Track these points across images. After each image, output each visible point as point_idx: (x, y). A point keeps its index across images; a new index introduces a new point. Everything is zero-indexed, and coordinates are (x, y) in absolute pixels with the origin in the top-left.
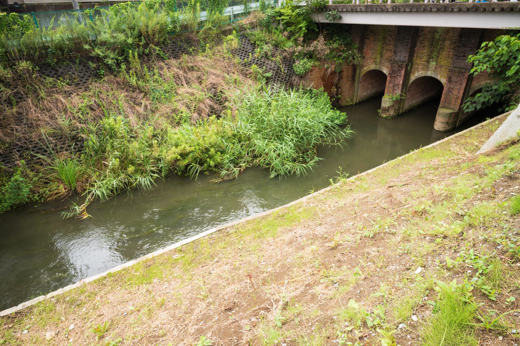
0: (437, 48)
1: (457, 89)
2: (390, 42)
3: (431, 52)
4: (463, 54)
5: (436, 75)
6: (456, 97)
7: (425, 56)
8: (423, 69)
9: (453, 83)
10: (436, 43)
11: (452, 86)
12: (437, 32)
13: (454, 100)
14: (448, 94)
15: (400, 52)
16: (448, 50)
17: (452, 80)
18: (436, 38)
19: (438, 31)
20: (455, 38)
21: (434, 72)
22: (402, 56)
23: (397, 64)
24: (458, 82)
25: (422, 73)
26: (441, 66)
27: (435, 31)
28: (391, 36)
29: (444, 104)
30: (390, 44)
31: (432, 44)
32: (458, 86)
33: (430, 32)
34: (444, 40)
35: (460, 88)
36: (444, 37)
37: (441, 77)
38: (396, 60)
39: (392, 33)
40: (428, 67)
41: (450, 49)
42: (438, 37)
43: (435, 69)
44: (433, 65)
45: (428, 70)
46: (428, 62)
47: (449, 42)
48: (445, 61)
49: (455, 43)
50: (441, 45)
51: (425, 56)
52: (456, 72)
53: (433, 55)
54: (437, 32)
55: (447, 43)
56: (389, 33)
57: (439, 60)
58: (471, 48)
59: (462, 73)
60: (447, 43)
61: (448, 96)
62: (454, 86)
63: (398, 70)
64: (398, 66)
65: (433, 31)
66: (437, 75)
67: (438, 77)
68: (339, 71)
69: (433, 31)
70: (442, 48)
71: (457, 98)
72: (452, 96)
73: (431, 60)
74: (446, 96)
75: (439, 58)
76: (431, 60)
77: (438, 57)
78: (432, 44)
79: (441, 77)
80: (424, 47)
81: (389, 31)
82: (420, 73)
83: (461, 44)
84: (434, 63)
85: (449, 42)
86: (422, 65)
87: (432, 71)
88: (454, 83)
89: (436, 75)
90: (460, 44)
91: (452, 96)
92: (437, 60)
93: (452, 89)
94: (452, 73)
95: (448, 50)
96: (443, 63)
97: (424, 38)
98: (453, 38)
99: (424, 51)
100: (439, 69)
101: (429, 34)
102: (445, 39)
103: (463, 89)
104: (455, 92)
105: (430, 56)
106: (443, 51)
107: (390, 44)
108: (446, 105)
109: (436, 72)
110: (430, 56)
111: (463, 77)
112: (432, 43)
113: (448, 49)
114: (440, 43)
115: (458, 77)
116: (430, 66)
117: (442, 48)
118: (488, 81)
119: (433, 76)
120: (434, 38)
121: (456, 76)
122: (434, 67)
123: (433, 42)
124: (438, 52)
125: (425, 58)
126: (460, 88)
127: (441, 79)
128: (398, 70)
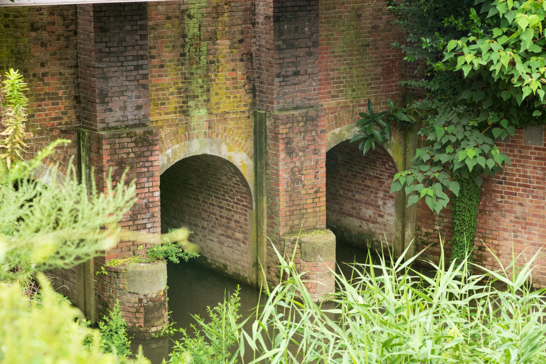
0: (198, 63)
1: (311, 168)
2: (43, 65)
3: (186, 80)
4: (294, 69)
5: (214, 147)
6: (312, 191)
7: (172, 94)
8: (176, 137)
9: (297, 155)
10: (192, 49)
11: (298, 164)
12: (190, 17)
13: (310, 201)
14: (293, 189)
15: (122, 93)
16: (230, 66)
17: (294, 145)
18: (190, 35)
19: (192, 12)
20: (240, 28)
21: (207, 140)
22: (129, 105)
23: (129, 135)
24: (307, 148)
25: (174, 152)
26: (224, 117)
27: (183, 12)
28: (43, 45)
29: (290, 223)
30: (44, 75)
31: (183, 55)
32: (310, 160)
33: (169, 18)
34: (213, 38)
35: (317, 162)
36: (209, 29)
37: (229, 150)
38: (113, 124)
39: (45, 35)
40: (187, 127)
41: (233, 60)
42: (196, 30)
43: (210, 128)
44: (200, 118)
45: (189, 138)
46: (185, 112)
47: (228, 42)
48: (229, 97)
49: (241, 41)
50: (208, 54)
51: (172, 94)
52: (298, 122)
53: (193, 87)
54: (190, 17)
55: (223, 44)
56: (33, 34)
57: (214, 99)
58: (307, 50)
59: (313, 120)
60: (223, 44)
61: (294, 196)
62: (302, 163)
63: (139, 156)
64: (136, 142)
65: (178, 13)
66: (219, 147)
67: (224, 153)
68: (467, 113)
69: (178, 13)
70: (212, 62)
71: (316, 192)
72: (304, 192)
73: (191, 103)
74: (290, 196)
75: (212, 93)
76: (191, 103)
77: (208, 90)
78: (183, 55)
79: (229, 150)
80: (162, 66)
81: (34, 28)
82: (169, 151)
83: (284, 41)
84: (203, 112)
85: (228, 42)
86: (170, 126)
87: (202, 138)
88: (301, 154)
89: (214, 147)
90: (280, 43)
91: (304, 192)
92: (208, 100)
93: (300, 171)
94: (289, 125)
95: (230, 66)
96: (226, 105)
97: (156, 38)
98: (235, 29)
99: (166, 80)
100: (221, 126)
101: (168, 25)
102: (216, 34)
103: (324, 164)
104: (308, 179)
105: (186, 90)
106: (217, 70)
107: (44, 75)
108: (296, 222)
109: (214, 136)
110: (186, 90)
111: (316, 131)
112: (181, 50)
113: (227, 62)
114: (204, 49)
115: (305, 132)
116: (194, 123)
117: (212, 62)
118: (337, 131)
119: (209, 153)
120: (184, 36)
121: (300, 132)
122: (206, 124)
123: (183, 46)
124: (207, 76)
125: (173, 102)
126: (317, 162)
127: (232, 154)
128: (139, 156)
